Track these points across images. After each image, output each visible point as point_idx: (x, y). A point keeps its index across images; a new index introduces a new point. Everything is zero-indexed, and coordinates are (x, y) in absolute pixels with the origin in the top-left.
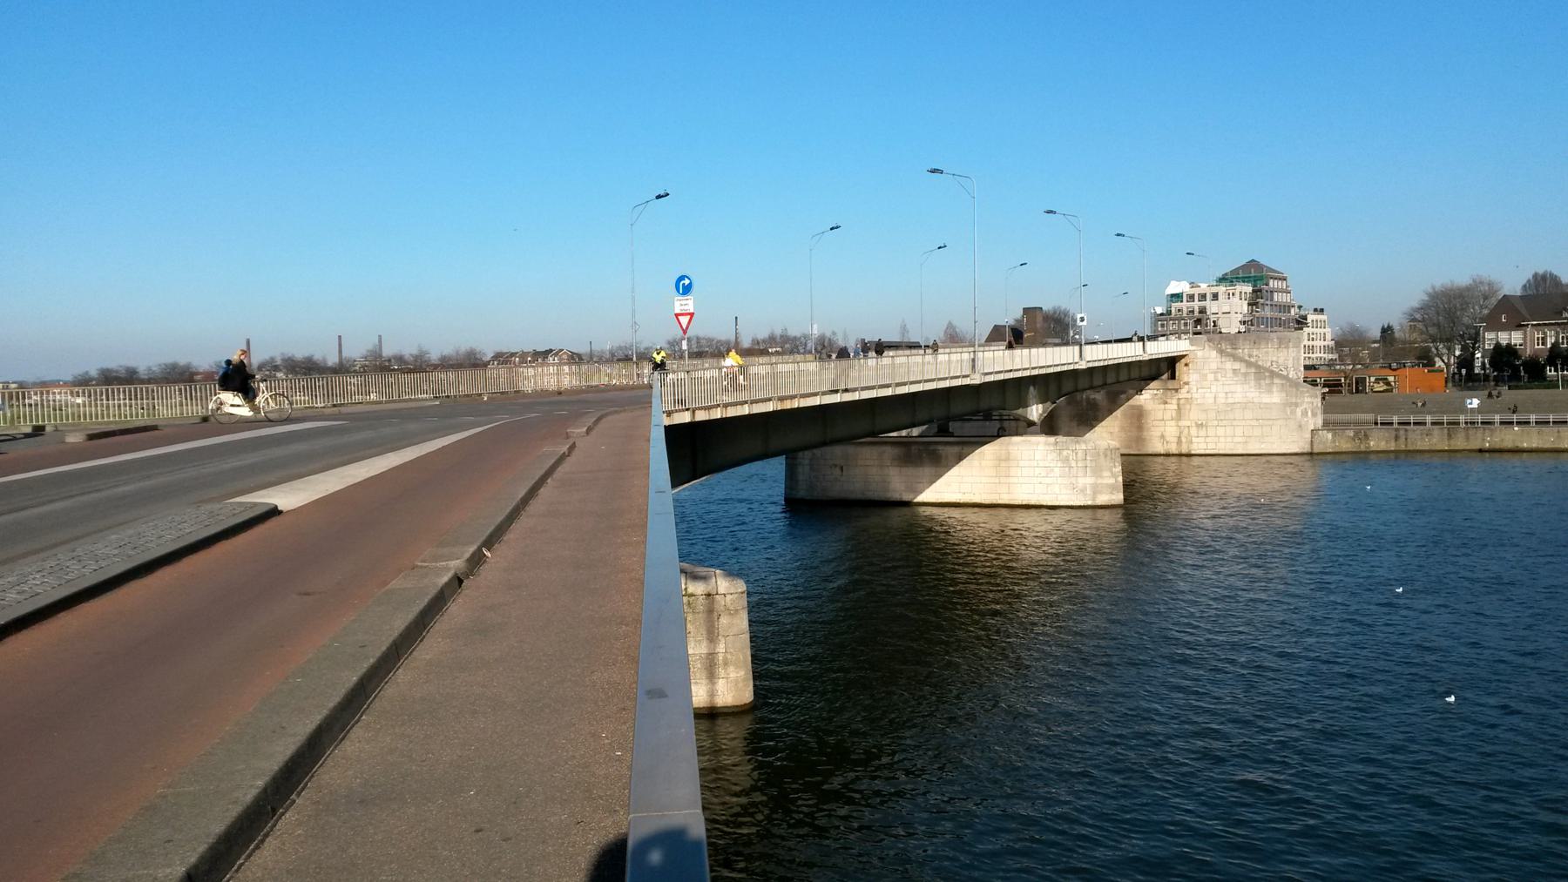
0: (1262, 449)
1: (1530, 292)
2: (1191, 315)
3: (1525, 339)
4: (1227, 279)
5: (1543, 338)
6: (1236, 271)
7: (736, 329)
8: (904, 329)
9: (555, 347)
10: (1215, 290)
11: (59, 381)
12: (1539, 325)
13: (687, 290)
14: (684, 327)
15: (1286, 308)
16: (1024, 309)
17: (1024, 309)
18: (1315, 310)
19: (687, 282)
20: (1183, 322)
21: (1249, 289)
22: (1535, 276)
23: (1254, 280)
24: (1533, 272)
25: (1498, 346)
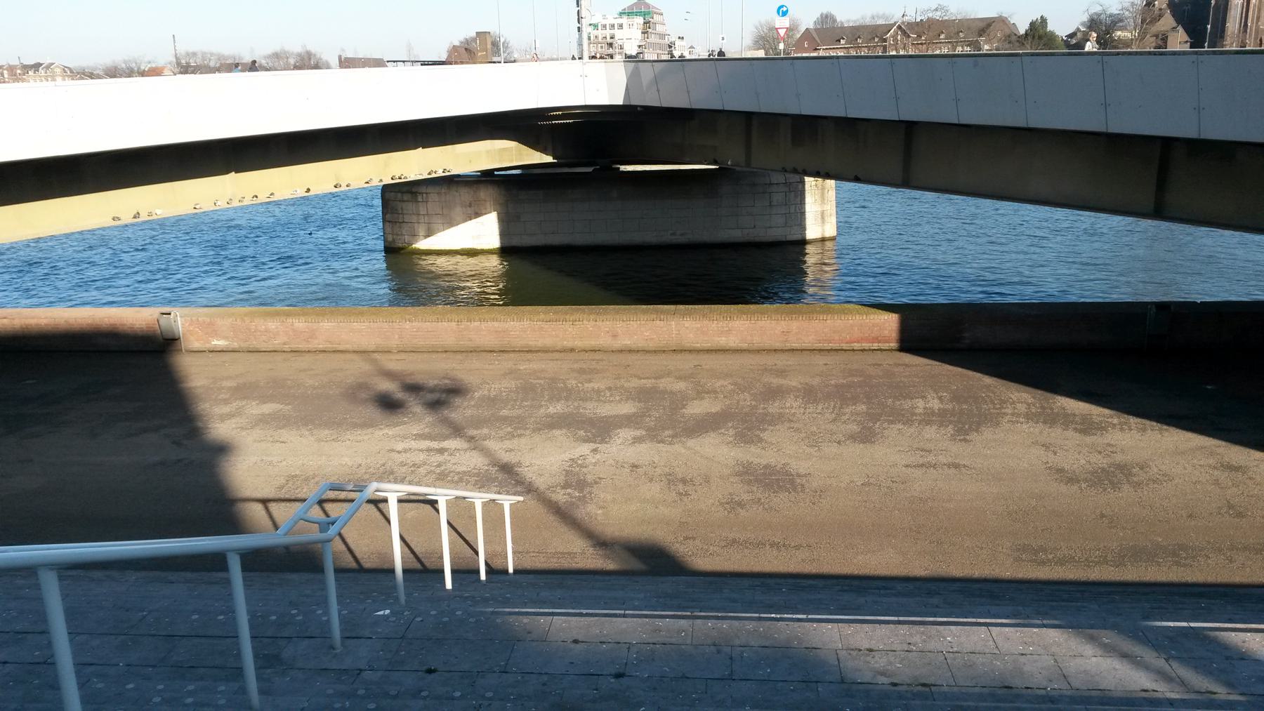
1: (818, 27)
2: (604, 40)
4: (625, 13)
6: (631, 7)
7: (175, 46)
8: (410, 49)
9: (47, 61)
10: (620, 21)
11: (243, 71)
12: (827, 49)
13: (784, 14)
15: (662, 36)
18: (679, 38)
19: (785, 9)
20: (600, 45)
21: (640, 20)
22: (822, 15)
23: (644, 14)
24: (1036, 16)
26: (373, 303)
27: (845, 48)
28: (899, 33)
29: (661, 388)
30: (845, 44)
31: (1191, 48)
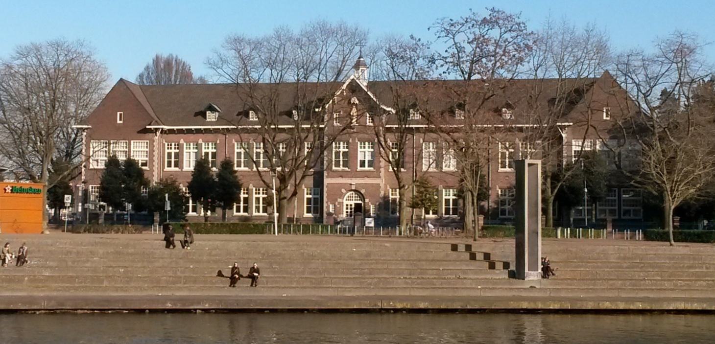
0: (703, 247)
3: (151, 154)
5: (177, 155)
12: (171, 132)
14: (640, 93)
16: (121, 80)
17: (121, 80)
22: (157, 60)
25: (112, 162)
26: (467, 261)
27: (216, 131)
28: (355, 100)
29: (623, 303)
30: (220, 120)
31: (360, 161)
